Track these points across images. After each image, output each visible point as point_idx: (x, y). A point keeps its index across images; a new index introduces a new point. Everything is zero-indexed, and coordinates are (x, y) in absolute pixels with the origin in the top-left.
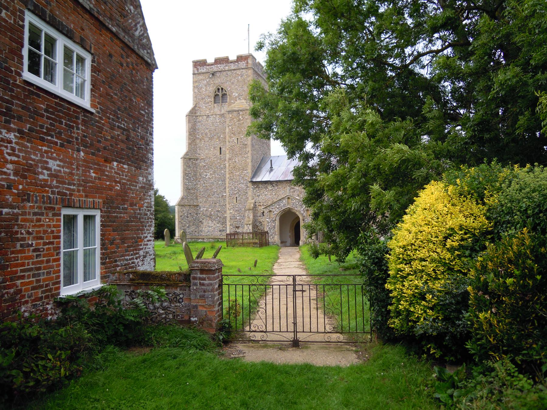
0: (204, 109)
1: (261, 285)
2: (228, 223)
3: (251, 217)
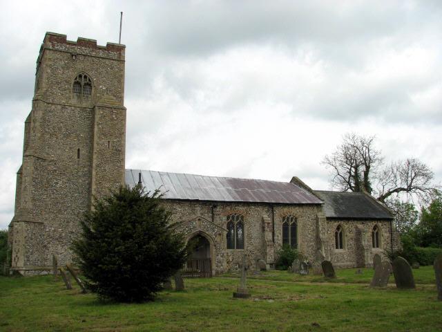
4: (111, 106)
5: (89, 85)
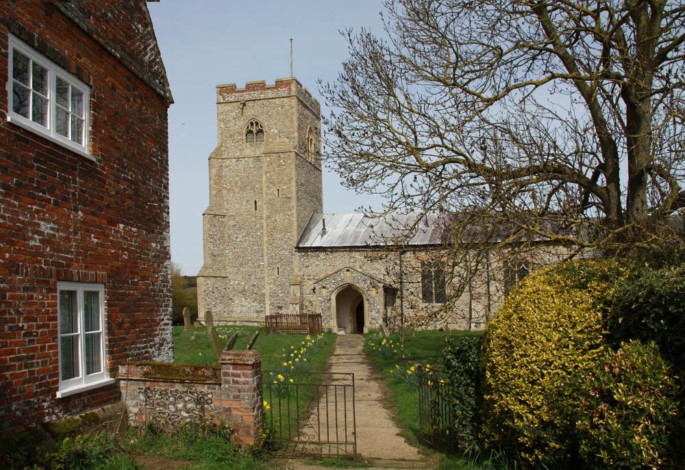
2: (268, 302)
3: (298, 294)
4: (277, 151)
5: (261, 131)
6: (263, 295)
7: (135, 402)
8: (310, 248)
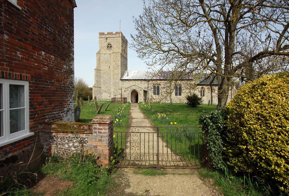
0: (103, 51)
1: (137, 132)
2: (112, 94)
3: (121, 92)
4: (115, 52)
5: (111, 47)
6: (111, 92)
7: (47, 143)
8: (124, 79)
